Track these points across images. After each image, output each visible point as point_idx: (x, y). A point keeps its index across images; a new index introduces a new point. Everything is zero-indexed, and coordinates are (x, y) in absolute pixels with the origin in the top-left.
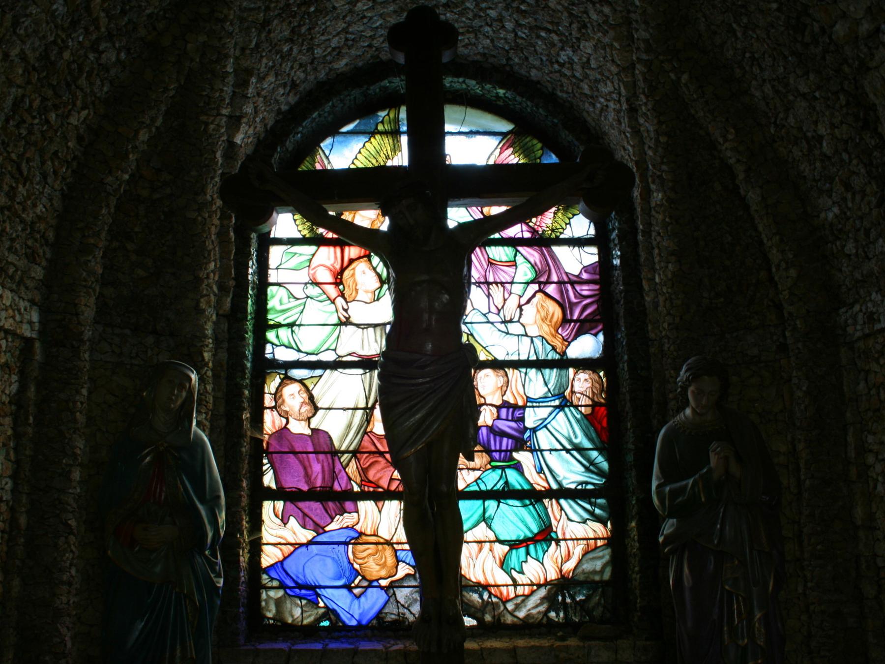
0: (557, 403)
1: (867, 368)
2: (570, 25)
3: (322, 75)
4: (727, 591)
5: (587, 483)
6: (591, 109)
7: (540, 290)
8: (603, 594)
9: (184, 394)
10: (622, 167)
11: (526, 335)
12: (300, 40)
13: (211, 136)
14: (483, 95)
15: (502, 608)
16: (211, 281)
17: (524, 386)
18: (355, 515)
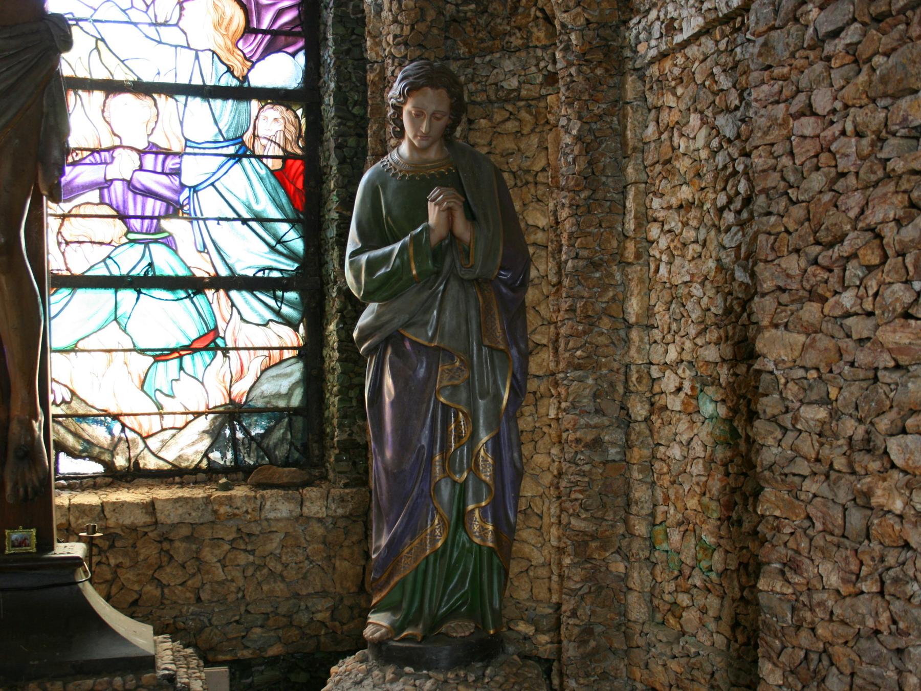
0: (232, 150)
1: (659, 104)
4: (442, 404)
5: (271, 269)
8: (290, 426)
11: (189, 47)
15: (141, 445)
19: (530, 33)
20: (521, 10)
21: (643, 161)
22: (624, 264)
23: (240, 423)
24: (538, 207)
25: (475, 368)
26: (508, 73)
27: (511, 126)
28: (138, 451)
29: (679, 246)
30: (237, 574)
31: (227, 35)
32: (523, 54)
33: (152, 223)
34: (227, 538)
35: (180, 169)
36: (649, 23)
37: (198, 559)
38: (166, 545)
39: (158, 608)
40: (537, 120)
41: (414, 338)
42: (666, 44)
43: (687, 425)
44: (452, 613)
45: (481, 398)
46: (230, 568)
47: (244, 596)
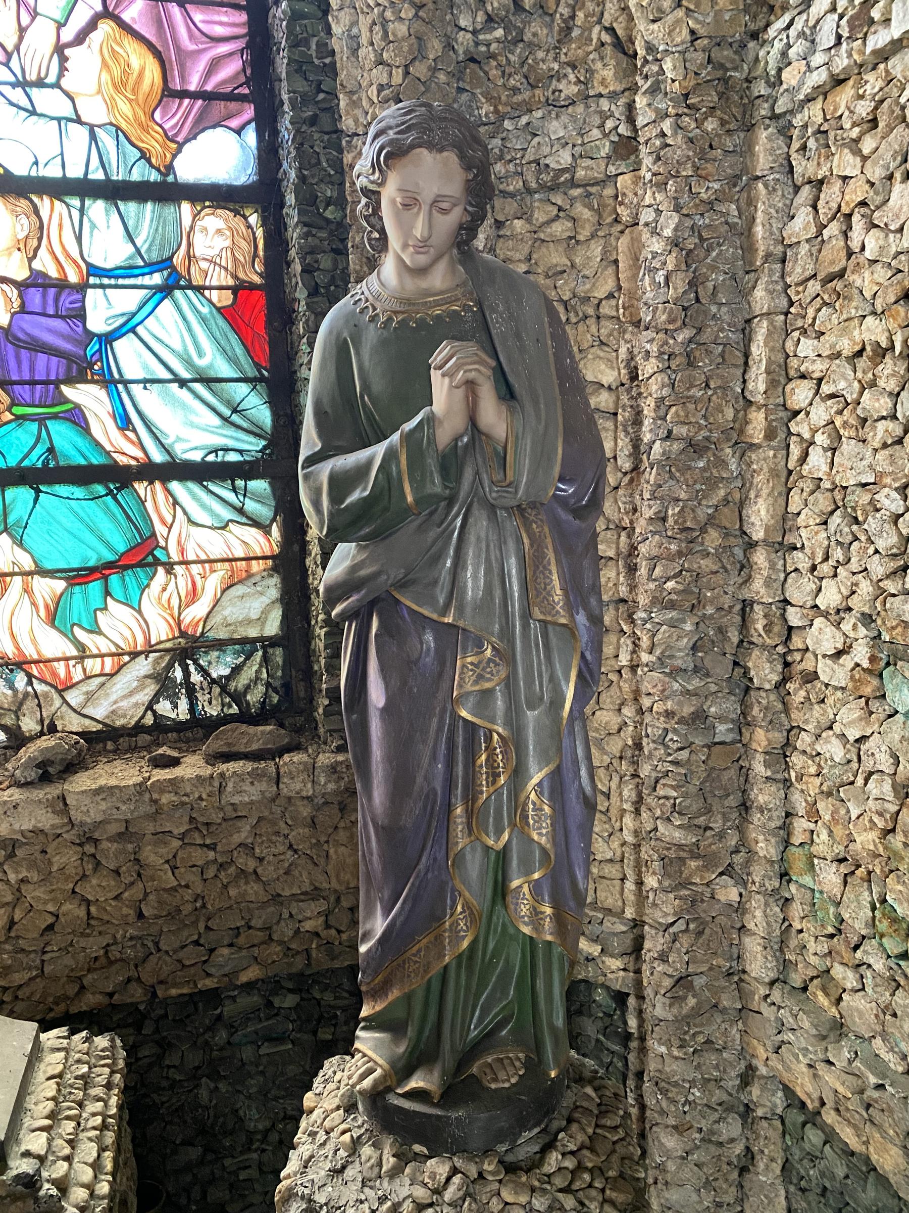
0: (157, 279)
4: (464, 719)
5: (226, 450)
8: (266, 659)
11: (79, 121)
15: (58, 702)
17: (79, 239)
19: (590, 71)
20: (576, 33)
21: (783, 276)
22: (744, 448)
23: (195, 662)
24: (602, 354)
25: (518, 657)
26: (557, 142)
27: (560, 229)
28: (53, 709)
29: (853, 421)
30: (193, 878)
31: (137, 100)
32: (580, 109)
33: (48, 391)
34: (176, 832)
35: (83, 308)
36: (811, 23)
37: (137, 860)
38: (89, 849)
39: (82, 934)
40: (600, 216)
41: (415, 607)
42: (850, 55)
43: (857, 714)
46: (183, 870)
47: (204, 906)
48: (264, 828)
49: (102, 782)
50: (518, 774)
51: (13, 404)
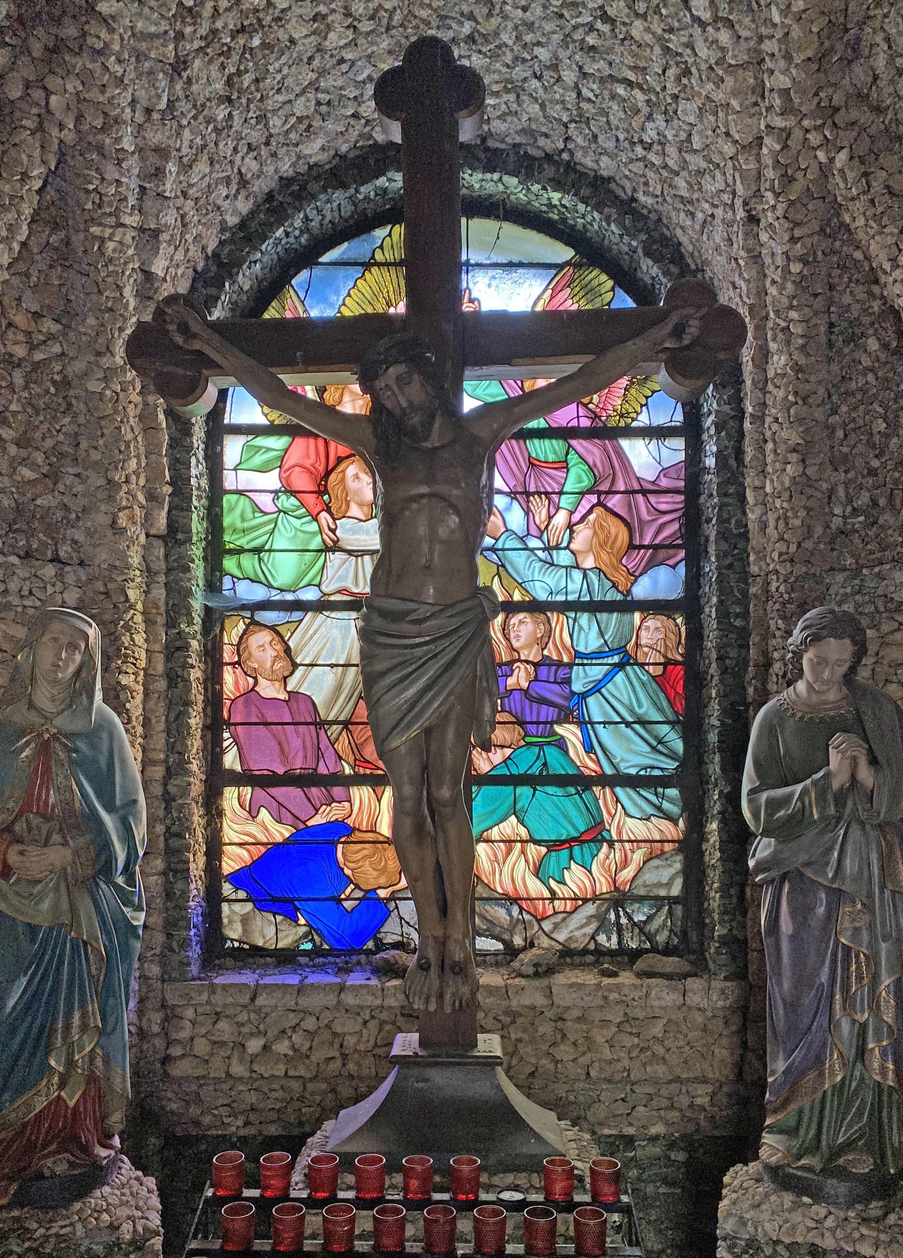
0: (616, 659)
2: (664, 71)
3: (286, 168)
5: (653, 768)
6: (689, 223)
7: (600, 504)
8: (670, 913)
9: (78, 658)
10: (729, 313)
11: (577, 567)
12: (244, 101)
13: (111, 260)
14: (529, 203)
15: (536, 928)
16: (133, 486)
17: (571, 636)
18: (346, 804)
44: (849, 1146)
45: (884, 941)
48: (673, 1027)
49: (573, 980)
50: (875, 979)
51: (526, 735)
